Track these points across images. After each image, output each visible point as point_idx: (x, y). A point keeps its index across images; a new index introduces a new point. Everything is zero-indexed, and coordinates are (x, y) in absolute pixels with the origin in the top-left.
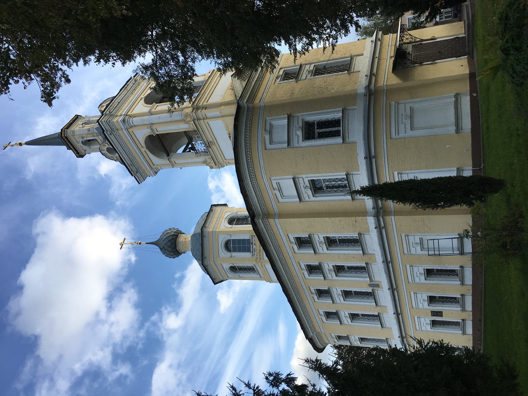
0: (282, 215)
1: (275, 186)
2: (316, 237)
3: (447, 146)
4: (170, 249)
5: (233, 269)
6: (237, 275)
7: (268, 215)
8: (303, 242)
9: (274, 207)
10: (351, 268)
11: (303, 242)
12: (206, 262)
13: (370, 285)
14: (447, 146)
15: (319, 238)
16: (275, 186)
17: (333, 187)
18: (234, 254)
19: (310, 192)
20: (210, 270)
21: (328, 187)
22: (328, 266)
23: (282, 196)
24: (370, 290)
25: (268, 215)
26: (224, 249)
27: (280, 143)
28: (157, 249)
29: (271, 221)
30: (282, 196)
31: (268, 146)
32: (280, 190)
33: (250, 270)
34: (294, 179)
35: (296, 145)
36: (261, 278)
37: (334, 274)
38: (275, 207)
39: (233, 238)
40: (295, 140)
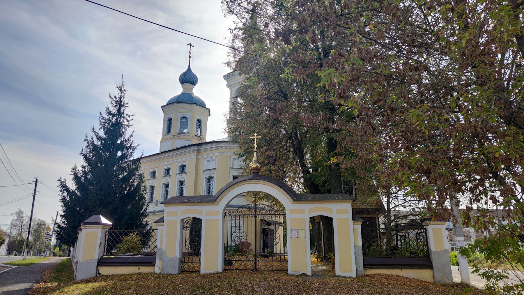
0: (197, 159)
1: (212, 159)
2: (185, 176)
3: (504, 3)
4: (185, 79)
5: (170, 120)
6: (166, 121)
7: (198, 152)
8: (183, 168)
9: (202, 156)
10: (167, 191)
11: (183, 168)
12: (175, 104)
13: (157, 201)
14: (504, 3)
15: (183, 177)
16: (212, 159)
17: (209, 188)
18: (179, 122)
19: (208, 176)
20: (169, 106)
21: (210, 185)
22: (168, 180)
23: (207, 161)
24: (154, 200)
25: (198, 152)
26: (183, 116)
27: (233, 164)
28: (185, 70)
29: (195, 153)
30: (207, 161)
31: (232, 158)
32: (210, 161)
33: (169, 131)
34: (215, 169)
35: (231, 171)
36: (163, 136)
37: (164, 182)
38: (202, 156)
39: (189, 122)
40: (233, 172)
